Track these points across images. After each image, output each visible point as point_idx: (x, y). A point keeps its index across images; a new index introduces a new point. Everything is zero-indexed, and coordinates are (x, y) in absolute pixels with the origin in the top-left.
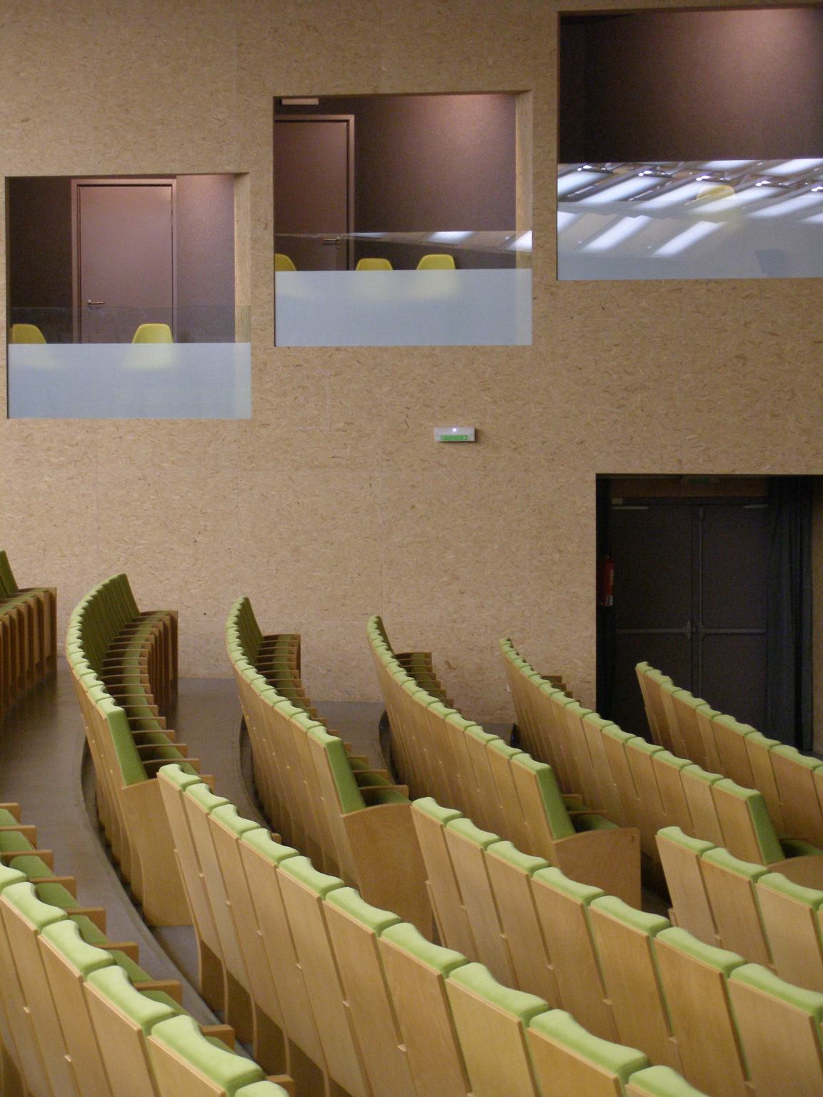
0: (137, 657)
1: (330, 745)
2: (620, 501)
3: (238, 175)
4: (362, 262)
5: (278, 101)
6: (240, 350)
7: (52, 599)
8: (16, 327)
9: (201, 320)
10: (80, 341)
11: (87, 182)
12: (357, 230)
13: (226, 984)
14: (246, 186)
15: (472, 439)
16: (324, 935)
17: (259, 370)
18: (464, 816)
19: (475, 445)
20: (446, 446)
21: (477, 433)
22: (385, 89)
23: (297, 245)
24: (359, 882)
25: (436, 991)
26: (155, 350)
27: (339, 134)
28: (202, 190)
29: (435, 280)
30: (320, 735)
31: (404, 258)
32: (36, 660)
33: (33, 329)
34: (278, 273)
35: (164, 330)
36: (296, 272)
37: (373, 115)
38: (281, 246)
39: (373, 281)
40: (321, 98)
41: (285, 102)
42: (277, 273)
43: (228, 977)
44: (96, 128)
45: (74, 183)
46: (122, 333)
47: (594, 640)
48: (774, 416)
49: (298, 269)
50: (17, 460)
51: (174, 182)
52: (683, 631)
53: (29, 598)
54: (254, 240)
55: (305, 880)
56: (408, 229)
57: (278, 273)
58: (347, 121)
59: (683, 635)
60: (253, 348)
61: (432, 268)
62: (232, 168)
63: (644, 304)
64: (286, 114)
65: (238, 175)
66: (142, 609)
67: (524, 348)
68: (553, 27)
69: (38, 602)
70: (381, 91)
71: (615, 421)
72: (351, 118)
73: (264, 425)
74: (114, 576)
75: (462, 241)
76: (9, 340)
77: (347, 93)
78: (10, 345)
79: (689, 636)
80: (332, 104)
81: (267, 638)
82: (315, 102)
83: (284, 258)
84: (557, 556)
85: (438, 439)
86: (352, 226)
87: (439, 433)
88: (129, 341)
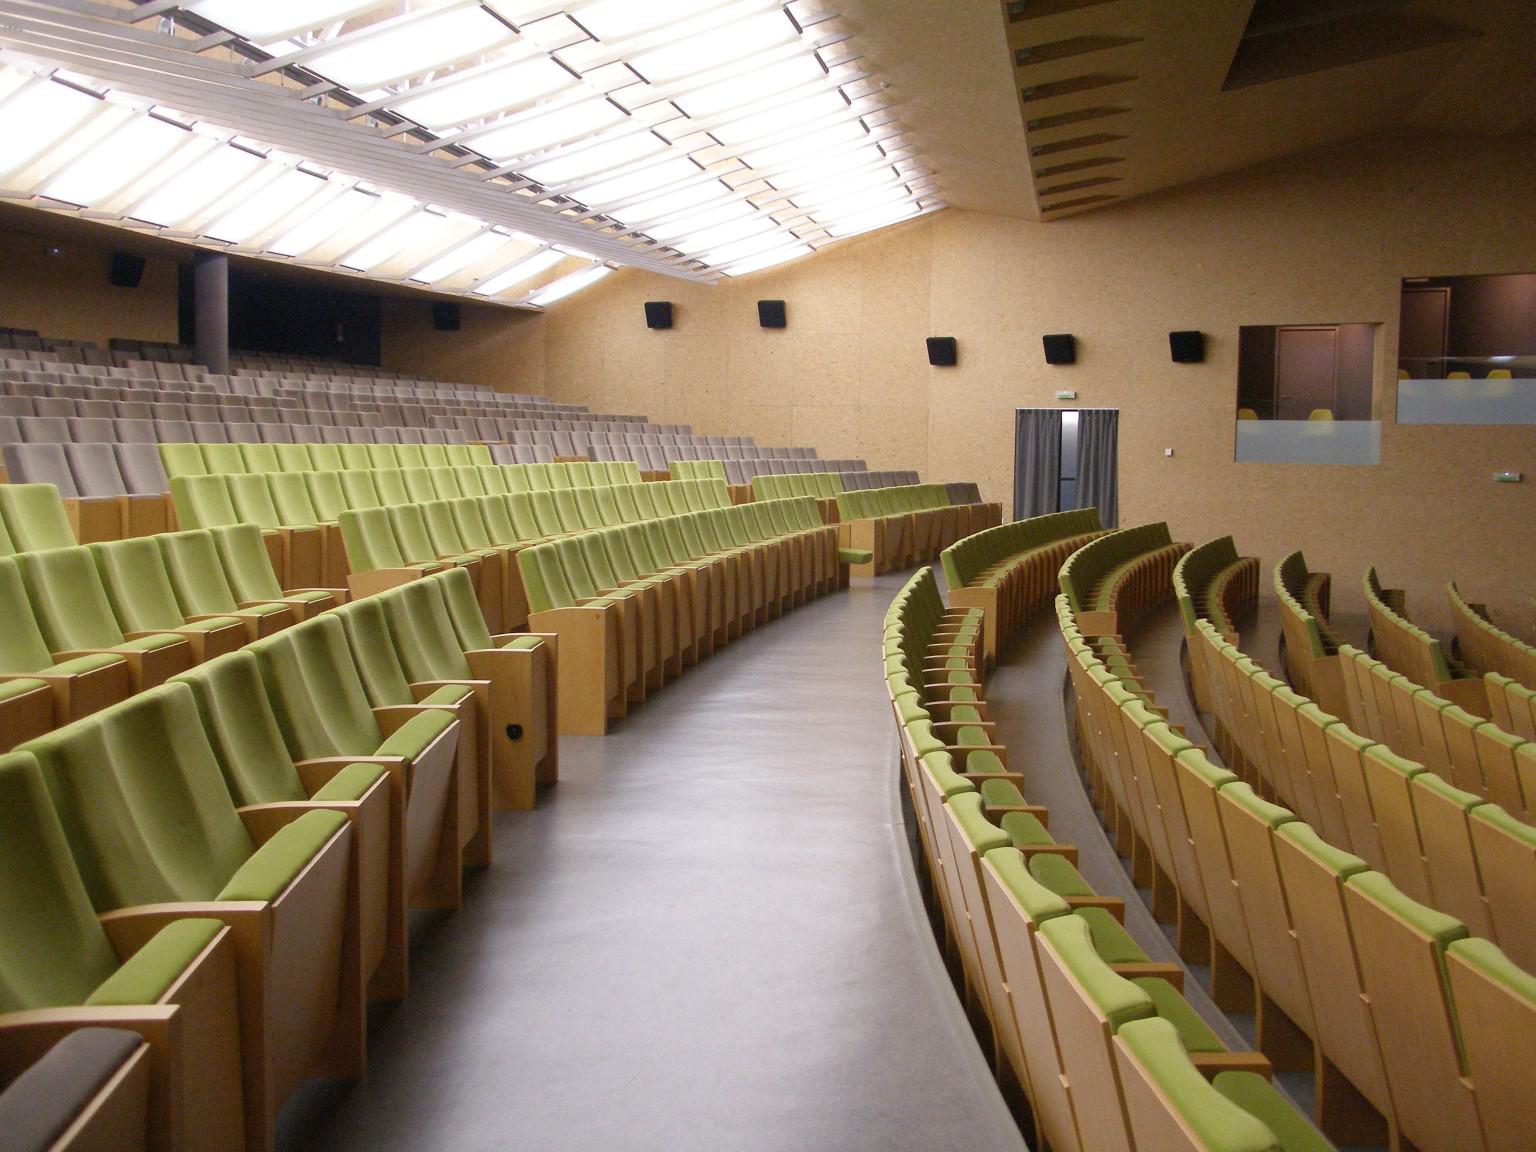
0: (1310, 596)
1: (1432, 644)
3: (1378, 324)
4: (1452, 374)
5: (1404, 280)
6: (1374, 425)
7: (1257, 563)
8: (1241, 411)
9: (1351, 406)
10: (1277, 419)
11: (1284, 329)
12: (1449, 355)
13: (1179, 910)
14: (1381, 332)
15: (1518, 479)
16: (1051, 1039)
17: (1385, 437)
18: (1516, 682)
22: (1472, 271)
23: (1414, 362)
24: (998, 1070)
25: (1510, 757)
26: (1323, 424)
27: (1442, 298)
29: (1499, 385)
30: (1427, 639)
31: (1479, 372)
32: (1248, 596)
33: (1251, 412)
34: (1077, 414)
35: (1328, 413)
37: (1464, 290)
38: (1402, 365)
39: (1458, 386)
40: (1430, 279)
41: (1408, 281)
43: (1182, 907)
45: (1277, 329)
46: (1302, 412)
51: (1337, 328)
53: (1245, 562)
55: (1431, 702)
56: (1477, 355)
57: (1077, 414)
58: (1446, 291)
62: (1373, 320)
64: (1409, 287)
65: (1378, 324)
66: (1309, 572)
69: (1251, 566)
70: (1470, 273)
72: (1449, 289)
74: (1295, 552)
75: (1512, 360)
76: (1237, 418)
80: (1436, 282)
81: (1385, 591)
82: (1426, 280)
83: (1404, 372)
86: (1445, 353)
87: (1497, 476)
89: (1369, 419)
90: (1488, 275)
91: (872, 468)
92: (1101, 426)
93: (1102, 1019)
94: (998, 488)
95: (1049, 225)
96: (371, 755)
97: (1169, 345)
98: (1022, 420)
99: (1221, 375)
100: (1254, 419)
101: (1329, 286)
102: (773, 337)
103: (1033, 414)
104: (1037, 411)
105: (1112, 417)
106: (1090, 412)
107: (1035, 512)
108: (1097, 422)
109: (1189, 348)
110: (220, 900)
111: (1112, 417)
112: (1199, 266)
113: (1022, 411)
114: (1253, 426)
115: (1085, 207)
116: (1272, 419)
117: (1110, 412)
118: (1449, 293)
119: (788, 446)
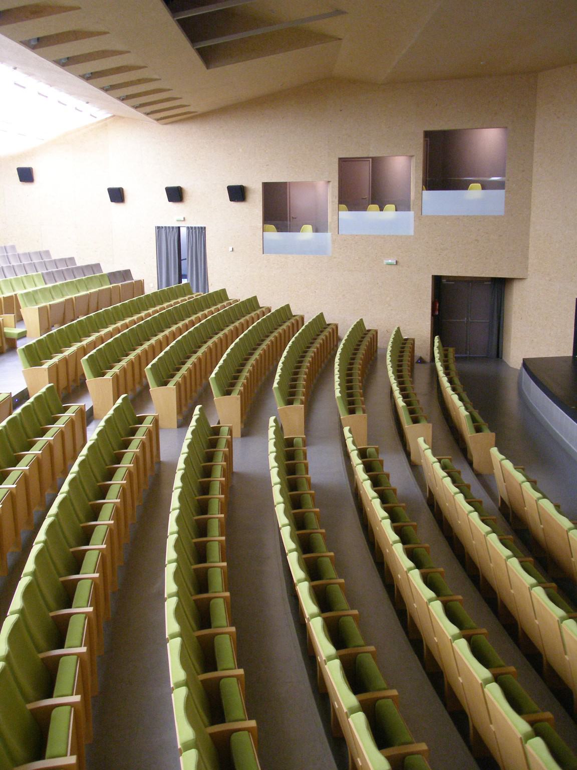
2: (445, 281)
3: (329, 182)
9: (402, 205)
17: (334, 241)
19: (396, 266)
20: (388, 266)
21: (396, 262)
23: (350, 198)
28: (321, 185)
29: (475, 192)
35: (393, 206)
36: (348, 212)
37: (376, 163)
42: (339, 212)
44: (287, 168)
47: (430, 326)
48: (486, 259)
49: (349, 211)
50: (266, 266)
52: (464, 320)
54: (333, 202)
59: (464, 322)
60: (332, 234)
61: (473, 189)
63: (448, 223)
64: (342, 161)
65: (329, 182)
67: (411, 236)
68: (422, 135)
71: (438, 259)
73: (335, 258)
76: (263, 231)
77: (422, 149)
78: (264, 233)
79: (466, 322)
84: (420, 300)
85: (385, 263)
87: (385, 262)
88: (299, 232)
89: (410, 211)
90: (467, 129)
91: (80, 263)
92: (199, 233)
93: (480, 681)
94: (147, 274)
95: (165, 126)
96: (15, 467)
97: (337, 165)
98: (158, 231)
99: (254, 206)
100: (377, 211)
101: (304, 160)
102: (27, 186)
103: (164, 229)
104: (165, 227)
105: (202, 230)
106: (192, 228)
107: (168, 284)
108: (196, 232)
109: (238, 194)
110: (55, 697)
111: (202, 230)
112: (241, 150)
113: (158, 228)
114: (273, 235)
115: (179, 118)
116: (287, 232)
117: (202, 228)
118: (371, 161)
119: (41, 250)
